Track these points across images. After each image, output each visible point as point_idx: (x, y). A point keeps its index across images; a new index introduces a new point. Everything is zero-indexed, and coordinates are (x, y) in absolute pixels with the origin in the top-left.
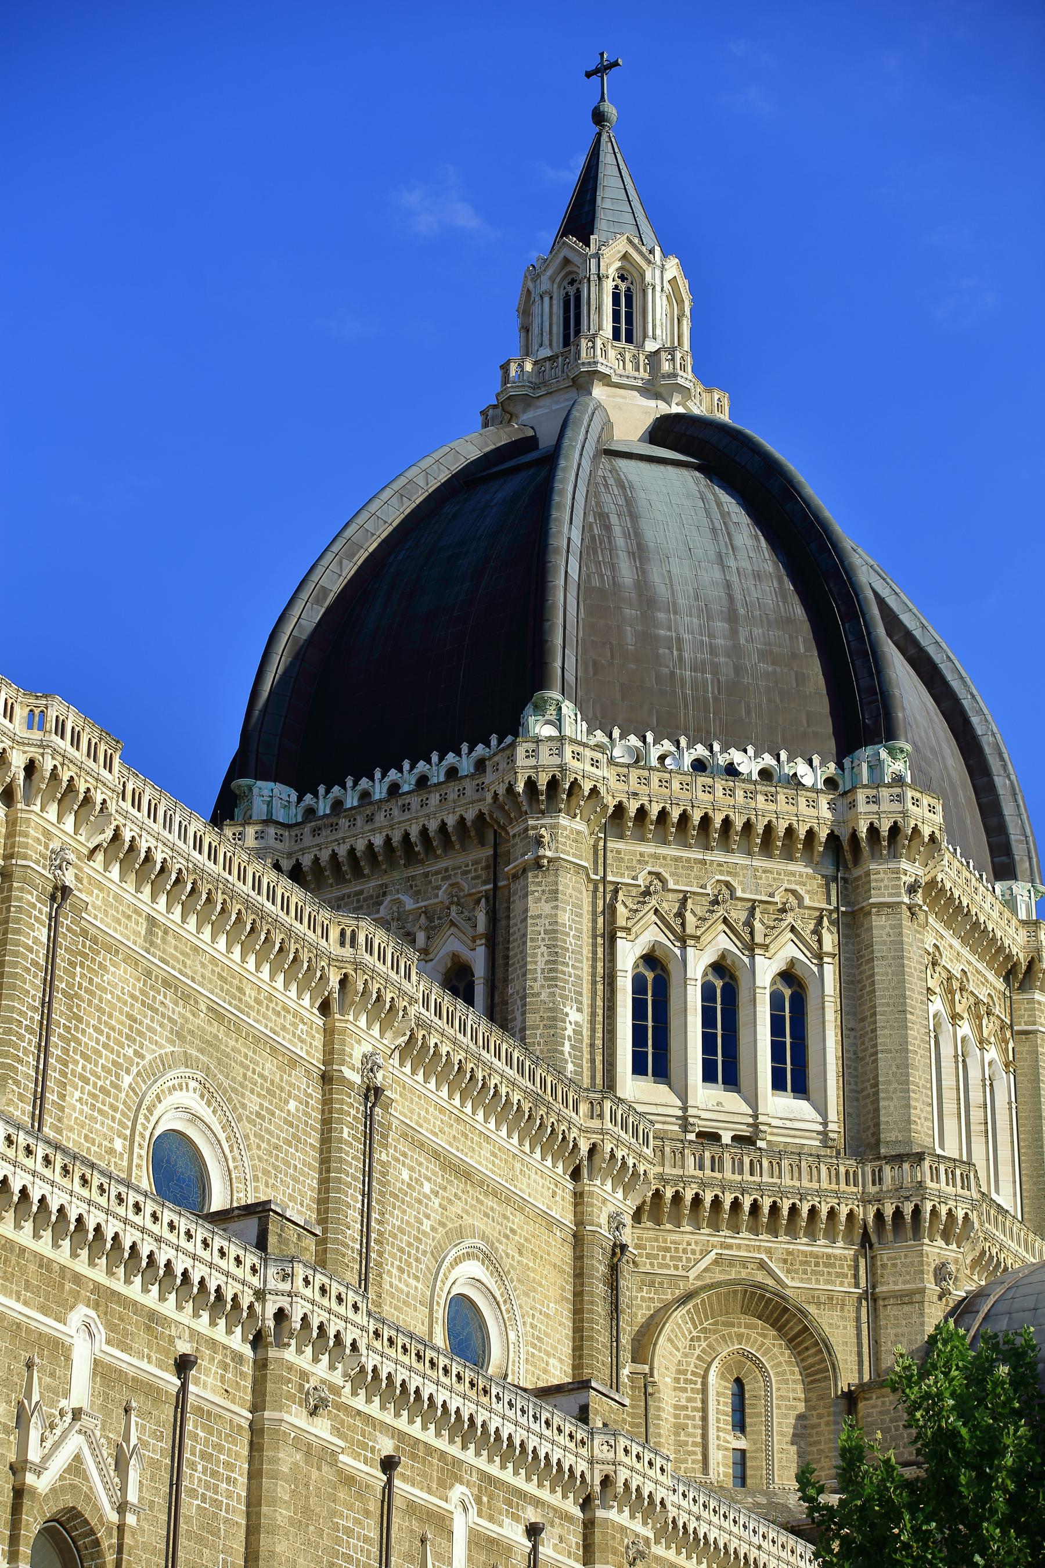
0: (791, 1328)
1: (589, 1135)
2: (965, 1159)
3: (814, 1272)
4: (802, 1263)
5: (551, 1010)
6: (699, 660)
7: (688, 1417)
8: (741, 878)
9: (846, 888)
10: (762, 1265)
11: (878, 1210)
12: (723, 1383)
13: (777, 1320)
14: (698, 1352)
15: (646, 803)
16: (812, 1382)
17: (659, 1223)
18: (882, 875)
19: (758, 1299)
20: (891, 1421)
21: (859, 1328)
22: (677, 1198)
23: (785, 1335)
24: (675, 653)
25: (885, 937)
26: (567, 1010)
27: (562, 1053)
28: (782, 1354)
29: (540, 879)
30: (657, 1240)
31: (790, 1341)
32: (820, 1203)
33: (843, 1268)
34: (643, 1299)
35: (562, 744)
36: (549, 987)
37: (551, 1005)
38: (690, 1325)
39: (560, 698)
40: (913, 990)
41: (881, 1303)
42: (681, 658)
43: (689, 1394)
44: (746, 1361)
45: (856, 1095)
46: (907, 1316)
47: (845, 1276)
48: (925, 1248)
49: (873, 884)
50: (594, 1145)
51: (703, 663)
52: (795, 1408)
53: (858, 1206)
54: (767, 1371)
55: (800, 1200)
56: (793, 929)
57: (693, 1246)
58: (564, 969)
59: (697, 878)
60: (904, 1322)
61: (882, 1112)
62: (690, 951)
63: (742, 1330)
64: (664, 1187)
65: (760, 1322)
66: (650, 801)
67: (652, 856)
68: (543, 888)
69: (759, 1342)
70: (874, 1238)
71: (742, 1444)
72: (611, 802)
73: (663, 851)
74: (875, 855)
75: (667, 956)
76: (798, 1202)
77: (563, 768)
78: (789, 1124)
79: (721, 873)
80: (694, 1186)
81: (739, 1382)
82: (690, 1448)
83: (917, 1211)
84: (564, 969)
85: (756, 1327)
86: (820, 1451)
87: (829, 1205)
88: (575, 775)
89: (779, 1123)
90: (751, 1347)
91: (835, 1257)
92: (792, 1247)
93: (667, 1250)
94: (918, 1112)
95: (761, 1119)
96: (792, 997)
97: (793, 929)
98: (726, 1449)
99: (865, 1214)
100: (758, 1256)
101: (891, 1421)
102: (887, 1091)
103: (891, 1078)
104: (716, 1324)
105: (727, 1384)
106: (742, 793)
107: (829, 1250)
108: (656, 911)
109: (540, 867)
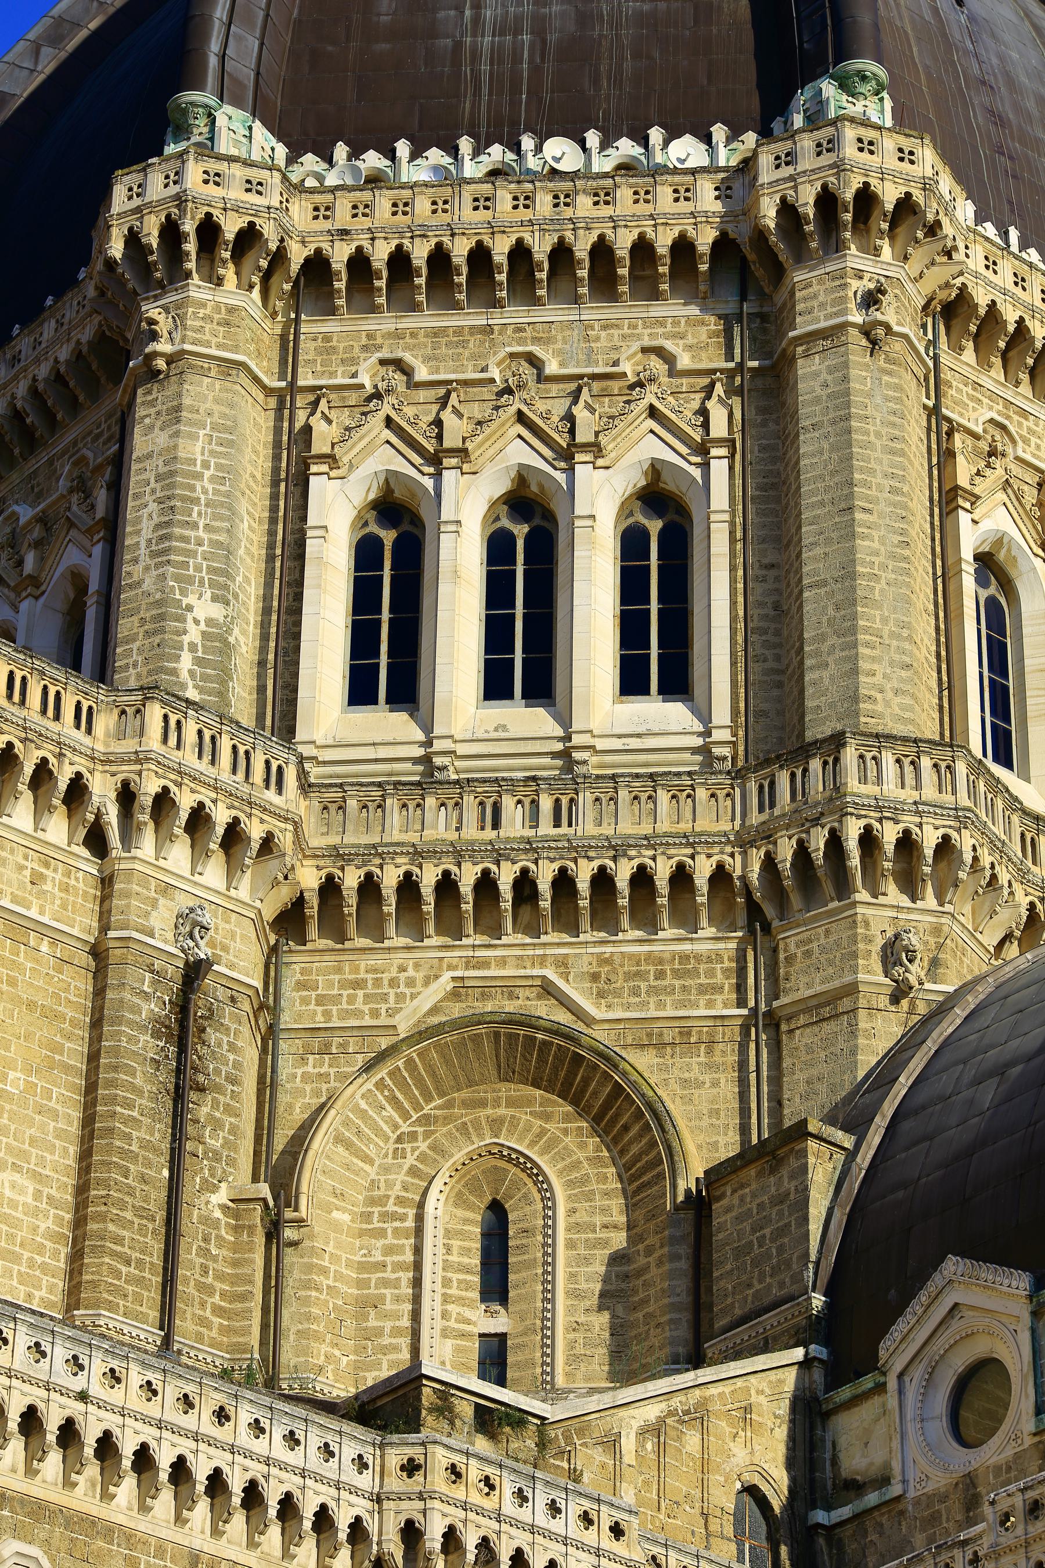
0: (595, 1093)
1: (114, 769)
2: (947, 740)
3: (652, 990)
4: (629, 976)
5: (159, 603)
6: (511, 16)
7: (385, 1283)
8: (559, 345)
9: (765, 331)
10: (547, 989)
11: (768, 854)
12: (460, 1213)
13: (568, 1083)
14: (410, 1160)
15: (366, 244)
16: (636, 1193)
17: (341, 937)
18: (815, 288)
19: (524, 1047)
20: (754, 1230)
21: (743, 1083)
22: (369, 888)
23: (588, 1113)
24: (468, 13)
25: (819, 391)
26: (191, 599)
27: (174, 672)
28: (582, 1146)
29: (154, 396)
30: (339, 970)
31: (597, 1120)
32: (654, 858)
33: (714, 976)
34: (306, 1078)
35: (183, 162)
36: (157, 566)
37: (158, 596)
38: (390, 1111)
39: (211, 100)
40: (872, 472)
41: (784, 1027)
42: (477, 20)
43: (390, 1240)
44: (509, 1166)
45: (777, 678)
46: (828, 1042)
47: (718, 989)
48: (860, 910)
49: (800, 307)
50: (126, 784)
51: (518, 19)
52: (605, 1243)
53: (732, 855)
54: (547, 1180)
55: (615, 859)
56: (653, 412)
57: (411, 972)
58: (187, 533)
59: (473, 357)
60: (823, 1055)
61: (809, 691)
62: (449, 477)
63: (502, 1111)
64: (342, 869)
65: (538, 1092)
66: (373, 239)
67: (389, 335)
68: (159, 407)
69: (535, 1130)
70: (769, 911)
71: (499, 1323)
72: (297, 255)
73: (411, 322)
74: (801, 255)
75: (413, 495)
76: (610, 863)
77: (180, 200)
78: (634, 743)
79: (521, 341)
80: (399, 860)
81: (497, 1211)
82: (386, 1341)
83: (835, 843)
84: (187, 533)
85: (529, 1102)
86: (648, 1316)
87: (673, 862)
88: (206, 209)
89: (617, 744)
90: (520, 1140)
91: (698, 958)
92: (608, 949)
93: (358, 984)
94: (878, 679)
95: (577, 740)
96: (662, 535)
97: (653, 412)
98: (463, 1335)
99: (745, 866)
100: (536, 972)
101: (754, 1230)
102: (817, 653)
103: (825, 629)
104: (449, 1105)
105: (470, 1215)
106: (549, 198)
107: (687, 947)
108: (389, 422)
109: (154, 374)
